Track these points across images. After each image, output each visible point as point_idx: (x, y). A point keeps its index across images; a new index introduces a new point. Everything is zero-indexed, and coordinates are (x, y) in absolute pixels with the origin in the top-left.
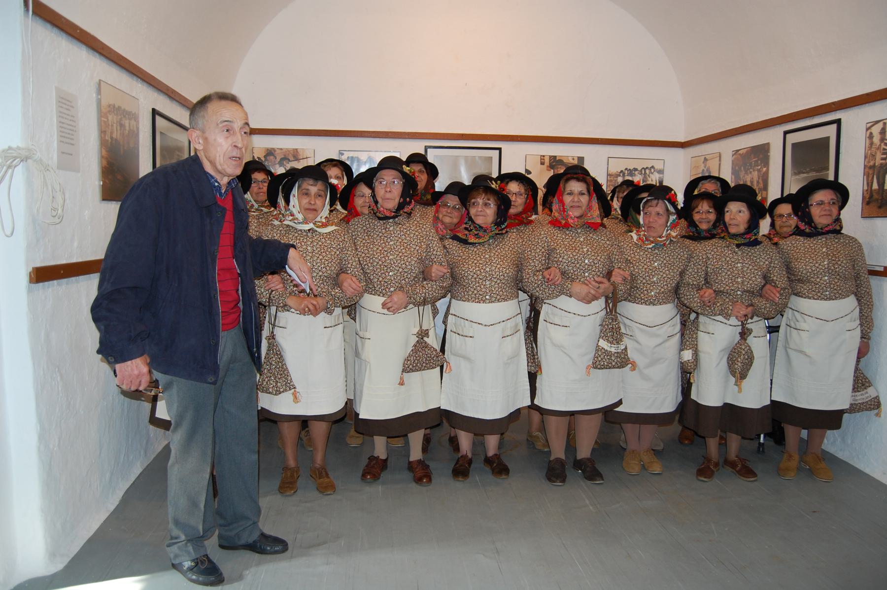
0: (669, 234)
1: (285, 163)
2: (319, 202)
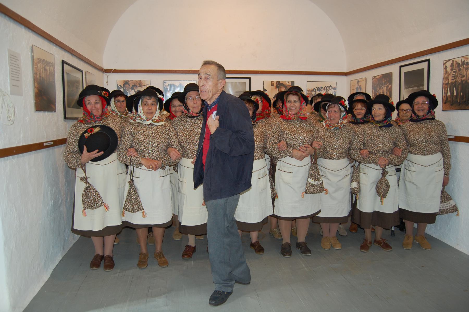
0: (342, 122)
1: (134, 88)
2: (153, 108)
